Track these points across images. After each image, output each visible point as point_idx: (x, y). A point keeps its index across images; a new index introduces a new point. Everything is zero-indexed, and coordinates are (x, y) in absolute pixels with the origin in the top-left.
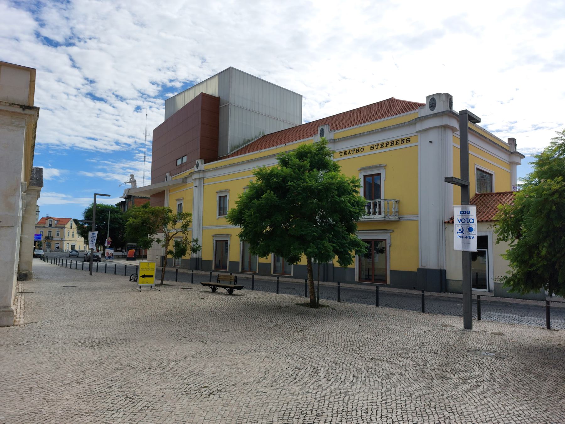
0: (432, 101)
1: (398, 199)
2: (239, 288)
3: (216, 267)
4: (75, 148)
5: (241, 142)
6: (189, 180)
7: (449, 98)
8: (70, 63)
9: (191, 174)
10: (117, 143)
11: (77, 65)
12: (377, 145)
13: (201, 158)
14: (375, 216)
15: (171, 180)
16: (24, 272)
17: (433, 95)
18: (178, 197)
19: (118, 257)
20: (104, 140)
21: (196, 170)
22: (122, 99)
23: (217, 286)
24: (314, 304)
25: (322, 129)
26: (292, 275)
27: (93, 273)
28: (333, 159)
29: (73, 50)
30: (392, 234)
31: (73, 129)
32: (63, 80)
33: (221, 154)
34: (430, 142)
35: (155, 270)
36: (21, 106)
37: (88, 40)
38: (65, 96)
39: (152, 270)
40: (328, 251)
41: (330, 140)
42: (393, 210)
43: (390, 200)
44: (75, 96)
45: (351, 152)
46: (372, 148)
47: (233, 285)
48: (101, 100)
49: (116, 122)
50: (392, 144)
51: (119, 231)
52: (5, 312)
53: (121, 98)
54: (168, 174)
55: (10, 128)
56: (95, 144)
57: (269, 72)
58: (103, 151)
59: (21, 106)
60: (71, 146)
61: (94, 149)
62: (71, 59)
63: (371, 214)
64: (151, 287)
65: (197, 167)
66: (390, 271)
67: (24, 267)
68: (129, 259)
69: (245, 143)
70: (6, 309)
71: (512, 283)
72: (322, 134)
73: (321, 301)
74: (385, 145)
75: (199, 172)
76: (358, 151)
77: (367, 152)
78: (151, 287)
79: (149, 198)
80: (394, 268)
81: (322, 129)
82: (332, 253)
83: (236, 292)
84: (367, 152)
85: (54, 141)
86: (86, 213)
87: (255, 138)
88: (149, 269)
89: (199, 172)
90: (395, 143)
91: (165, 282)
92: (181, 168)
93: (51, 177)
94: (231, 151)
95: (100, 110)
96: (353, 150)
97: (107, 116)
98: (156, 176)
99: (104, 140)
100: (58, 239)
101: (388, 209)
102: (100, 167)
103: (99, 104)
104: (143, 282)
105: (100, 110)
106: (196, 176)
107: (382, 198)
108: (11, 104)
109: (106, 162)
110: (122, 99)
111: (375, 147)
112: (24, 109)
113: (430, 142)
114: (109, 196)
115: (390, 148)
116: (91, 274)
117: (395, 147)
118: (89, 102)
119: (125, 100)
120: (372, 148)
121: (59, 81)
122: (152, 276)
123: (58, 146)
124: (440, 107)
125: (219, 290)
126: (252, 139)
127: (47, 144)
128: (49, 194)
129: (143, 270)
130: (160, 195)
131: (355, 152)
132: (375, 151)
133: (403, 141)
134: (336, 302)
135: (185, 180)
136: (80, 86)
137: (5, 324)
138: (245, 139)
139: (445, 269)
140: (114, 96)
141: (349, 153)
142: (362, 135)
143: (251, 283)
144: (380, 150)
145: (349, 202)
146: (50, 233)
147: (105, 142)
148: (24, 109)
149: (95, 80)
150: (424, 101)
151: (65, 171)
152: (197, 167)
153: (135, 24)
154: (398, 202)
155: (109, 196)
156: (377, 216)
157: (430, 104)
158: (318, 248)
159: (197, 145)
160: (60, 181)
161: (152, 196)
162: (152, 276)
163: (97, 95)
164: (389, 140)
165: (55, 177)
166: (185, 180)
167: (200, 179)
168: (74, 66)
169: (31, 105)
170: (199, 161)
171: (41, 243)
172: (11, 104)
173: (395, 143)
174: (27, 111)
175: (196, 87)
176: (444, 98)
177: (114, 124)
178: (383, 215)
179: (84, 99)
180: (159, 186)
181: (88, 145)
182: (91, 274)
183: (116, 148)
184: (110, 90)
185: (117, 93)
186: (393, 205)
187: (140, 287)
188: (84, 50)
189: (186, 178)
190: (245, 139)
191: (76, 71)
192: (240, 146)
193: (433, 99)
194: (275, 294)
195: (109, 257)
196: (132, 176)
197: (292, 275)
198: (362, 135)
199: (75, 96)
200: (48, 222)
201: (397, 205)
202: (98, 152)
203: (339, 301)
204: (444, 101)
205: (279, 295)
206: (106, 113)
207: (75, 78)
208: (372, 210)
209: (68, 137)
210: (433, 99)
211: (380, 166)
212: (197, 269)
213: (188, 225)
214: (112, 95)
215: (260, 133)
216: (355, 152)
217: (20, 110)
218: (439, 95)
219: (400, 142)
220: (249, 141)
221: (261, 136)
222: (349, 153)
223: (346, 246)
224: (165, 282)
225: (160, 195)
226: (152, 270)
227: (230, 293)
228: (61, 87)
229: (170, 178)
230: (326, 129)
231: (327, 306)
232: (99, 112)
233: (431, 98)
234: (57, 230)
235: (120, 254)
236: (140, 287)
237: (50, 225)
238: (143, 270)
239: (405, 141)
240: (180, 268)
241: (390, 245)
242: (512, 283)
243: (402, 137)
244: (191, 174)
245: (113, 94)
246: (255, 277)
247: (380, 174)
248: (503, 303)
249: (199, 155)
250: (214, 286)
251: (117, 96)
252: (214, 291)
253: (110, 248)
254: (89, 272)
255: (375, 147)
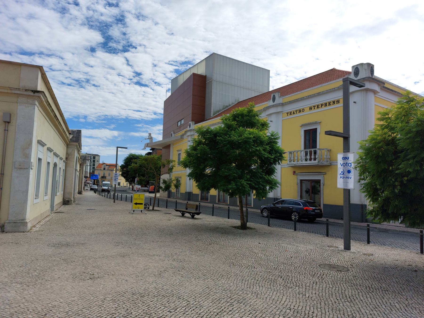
0: (356, 69)
1: (329, 148)
2: (198, 214)
3: (201, 199)
4: (129, 118)
5: (221, 108)
6: (185, 137)
7: (371, 67)
8: (126, 62)
9: (186, 132)
10: (155, 113)
11: (130, 64)
12: (314, 107)
13: (192, 121)
14: (311, 162)
15: (175, 136)
16: (67, 199)
17: (357, 65)
18: (178, 149)
19: (145, 191)
20: (147, 112)
21: (189, 129)
22: (159, 84)
23: (185, 212)
24: (244, 227)
25: (274, 96)
26: (252, 206)
27: (116, 201)
28: (263, 117)
29: (127, 54)
30: (325, 176)
31: (127, 105)
32: (121, 74)
33: (206, 117)
34: (355, 102)
35: (144, 199)
36: (32, 91)
37: (138, 47)
38: (123, 84)
39: (142, 199)
40: (245, 188)
41: (279, 104)
42: (325, 157)
43: (323, 149)
44: (129, 84)
45: (295, 113)
46: (311, 109)
47: (185, 210)
48: (146, 86)
49: (155, 99)
50: (326, 105)
51: (141, 171)
52: (22, 223)
53: (158, 84)
54: (172, 132)
55: (27, 105)
56: (141, 115)
57: (259, 60)
58: (146, 119)
59: (32, 91)
60: (126, 116)
61: (140, 117)
62: (127, 60)
63: (312, 160)
64: (141, 211)
65: (190, 127)
66: (324, 204)
67: (67, 196)
68: (150, 192)
69: (224, 109)
70: (23, 221)
71: (374, 213)
72: (274, 100)
73: (249, 224)
74: (320, 106)
75: (190, 130)
76: (300, 111)
77: (307, 112)
78: (141, 211)
79: (161, 149)
80: (325, 203)
81: (274, 96)
82: (247, 188)
83: (196, 216)
84: (307, 112)
85: (117, 114)
86: (125, 160)
87: (232, 104)
88: (140, 199)
89: (190, 130)
90: (328, 104)
91: (155, 208)
92: (180, 128)
93: (112, 137)
94: (214, 115)
95: (144, 92)
96: (296, 111)
97: (149, 96)
98: (165, 134)
99: (147, 112)
100: (109, 178)
101: (322, 156)
102: (144, 130)
103: (144, 88)
104: (136, 208)
105: (144, 92)
106: (189, 134)
107: (318, 147)
108: (26, 90)
109: (148, 126)
110: (159, 84)
111: (313, 108)
112: (34, 93)
113: (355, 102)
114: (127, 148)
115: (324, 108)
116: (114, 202)
117: (328, 107)
118: (138, 87)
119: (161, 85)
120: (311, 109)
121: (119, 75)
122: (142, 204)
123: (118, 116)
124: (362, 74)
125: (187, 215)
126: (230, 105)
127: (112, 116)
128: (111, 148)
129: (136, 199)
130: (168, 147)
131: (298, 112)
132: (313, 111)
133: (334, 102)
134: (266, 227)
135: (182, 136)
136: (131, 77)
137: (22, 230)
138: (224, 106)
139: (365, 204)
140: (153, 83)
141: (294, 113)
142: (302, 99)
143: (212, 210)
144: (317, 110)
145: (264, 150)
146: (104, 174)
147: (147, 113)
148: (34, 93)
149: (142, 73)
150: (350, 70)
151: (122, 133)
152: (190, 127)
153: (167, 33)
154: (330, 151)
155: (127, 148)
156: (313, 161)
157: (354, 73)
158: (236, 185)
159: (189, 111)
160: (118, 139)
161: (163, 148)
162: (142, 204)
163: (143, 83)
164: (323, 102)
165: (115, 137)
166: (182, 136)
167: (191, 135)
168: (128, 64)
169: (36, 90)
170: (191, 123)
171: (98, 181)
172: (26, 90)
173: (328, 104)
174: (36, 94)
175: (185, 73)
176: (366, 67)
177: (154, 101)
178: (317, 161)
179: (135, 86)
180: (168, 141)
181: (136, 116)
182: (114, 202)
183: (154, 117)
184: (151, 79)
185: (156, 81)
186: (325, 153)
187: (134, 211)
188: (135, 54)
189: (183, 135)
190: (224, 106)
191: (129, 68)
192: (220, 110)
193: (357, 68)
194: (227, 219)
195: (138, 191)
196: (150, 134)
197: (252, 206)
198: (302, 99)
199: (129, 84)
200: (103, 167)
201: (328, 153)
202: (142, 119)
203: (269, 225)
204: (365, 70)
205: (230, 220)
206: (149, 94)
207: (128, 72)
208: (308, 157)
209: (124, 111)
210: (357, 68)
211: (316, 123)
212: (189, 200)
213: (172, 169)
214: (152, 82)
215: (236, 101)
216: (298, 112)
217: (32, 94)
218: (362, 64)
219: (332, 103)
220: (227, 106)
221: (236, 103)
222: (294, 113)
223: (261, 184)
224: (155, 208)
225: (168, 147)
226: (142, 199)
227: (193, 217)
228: (120, 79)
229: (173, 135)
230: (277, 95)
231: (254, 229)
232: (144, 94)
233: (355, 67)
234: (109, 172)
235: (146, 188)
236: (134, 211)
237: (104, 169)
238: (136, 199)
239: (336, 102)
240: (179, 199)
241: (324, 185)
242: (374, 213)
243: (333, 100)
244: (186, 132)
245: (153, 81)
246: (215, 205)
247: (316, 129)
248: (410, 232)
249: (191, 119)
250: (183, 212)
251: (156, 83)
252: (183, 215)
253: (138, 184)
254: (113, 200)
255: (313, 108)
